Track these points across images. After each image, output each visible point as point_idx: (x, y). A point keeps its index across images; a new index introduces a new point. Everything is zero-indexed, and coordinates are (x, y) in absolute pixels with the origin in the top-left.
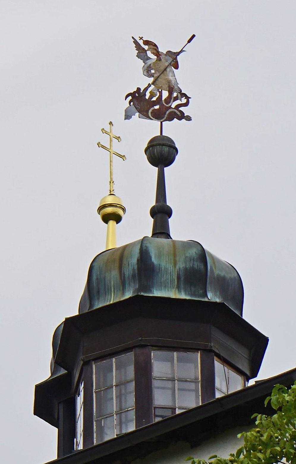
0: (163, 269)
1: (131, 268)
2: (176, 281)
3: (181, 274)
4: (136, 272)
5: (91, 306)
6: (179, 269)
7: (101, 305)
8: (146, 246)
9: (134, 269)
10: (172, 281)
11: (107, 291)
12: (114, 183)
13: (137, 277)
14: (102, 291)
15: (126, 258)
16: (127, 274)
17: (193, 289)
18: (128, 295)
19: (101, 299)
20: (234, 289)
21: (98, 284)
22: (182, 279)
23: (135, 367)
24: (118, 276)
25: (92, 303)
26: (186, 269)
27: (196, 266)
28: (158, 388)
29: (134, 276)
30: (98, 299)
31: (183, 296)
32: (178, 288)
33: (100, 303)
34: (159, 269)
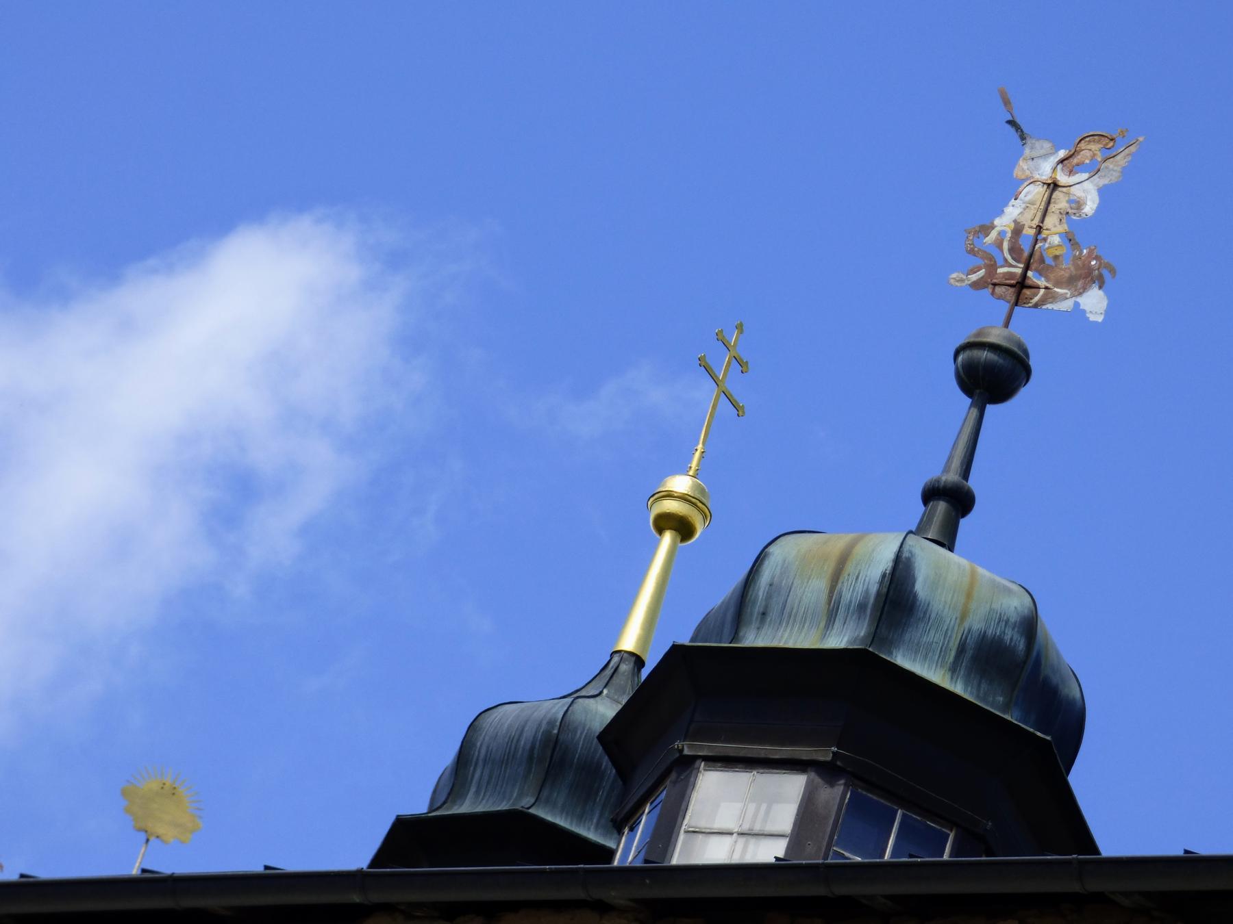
0: (933, 616)
1: (860, 588)
2: (953, 653)
3: (971, 642)
4: (872, 600)
5: (735, 637)
6: (969, 631)
7: (760, 643)
8: (911, 552)
9: (867, 592)
10: (944, 651)
11: (786, 616)
12: (991, 321)
13: (869, 611)
14: (773, 614)
15: (268, 872)
16: (847, 596)
17: (984, 686)
18: (837, 640)
19: (763, 632)
20: (1063, 724)
21: (769, 597)
22: (969, 653)
23: (618, 714)
24: (824, 597)
25: (741, 634)
26: (983, 637)
27: (1007, 638)
28: (765, 820)
29: (862, 607)
30: (540, 725)
31: (958, 688)
32: (954, 669)
33: (766, 626)
34: (925, 613)
